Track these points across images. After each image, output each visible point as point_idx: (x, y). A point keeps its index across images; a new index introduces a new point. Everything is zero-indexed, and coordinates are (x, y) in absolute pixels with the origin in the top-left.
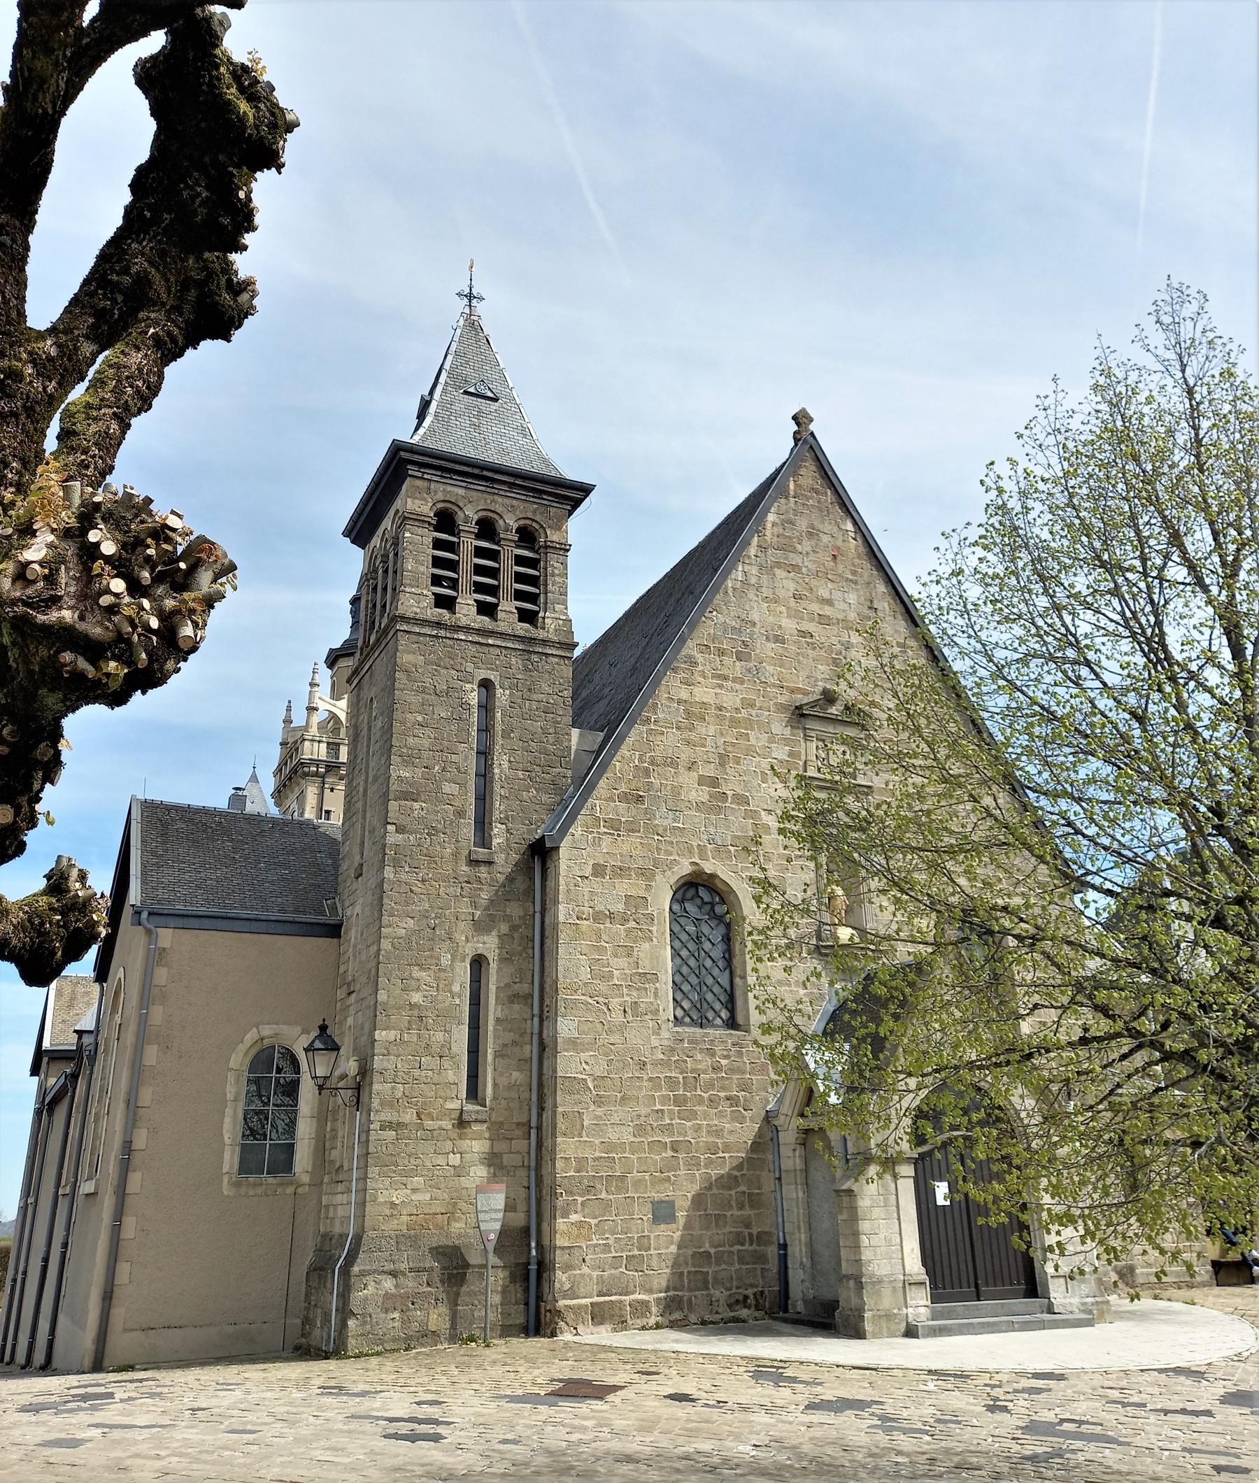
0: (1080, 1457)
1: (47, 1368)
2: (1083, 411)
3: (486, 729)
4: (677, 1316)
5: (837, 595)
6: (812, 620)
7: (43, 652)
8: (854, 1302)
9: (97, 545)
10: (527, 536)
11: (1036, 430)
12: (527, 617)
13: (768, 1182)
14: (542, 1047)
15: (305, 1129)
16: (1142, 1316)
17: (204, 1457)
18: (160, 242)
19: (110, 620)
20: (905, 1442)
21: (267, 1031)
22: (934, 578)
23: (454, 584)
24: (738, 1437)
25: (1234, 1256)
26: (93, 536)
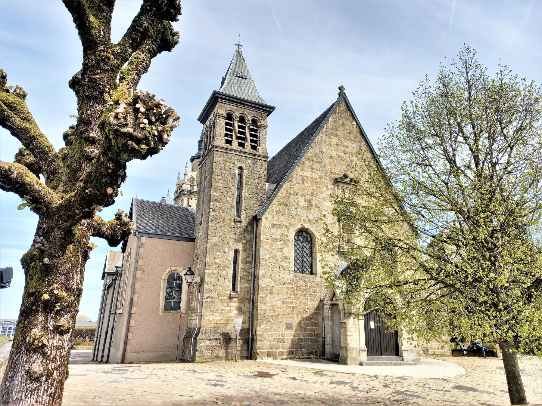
0: (411, 401)
1: (107, 362)
2: (434, 87)
3: (240, 182)
4: (292, 356)
5: (350, 145)
6: (341, 152)
7: (123, 141)
8: (345, 354)
9: (139, 109)
10: (254, 122)
11: (419, 92)
12: (254, 148)
13: (320, 319)
14: (255, 277)
15: (184, 297)
16: (427, 363)
17: (155, 387)
18: (152, 17)
19: (143, 132)
20: (360, 394)
21: (173, 268)
22: (384, 138)
23: (231, 136)
24: (310, 390)
25: (459, 348)
26: (138, 106)
